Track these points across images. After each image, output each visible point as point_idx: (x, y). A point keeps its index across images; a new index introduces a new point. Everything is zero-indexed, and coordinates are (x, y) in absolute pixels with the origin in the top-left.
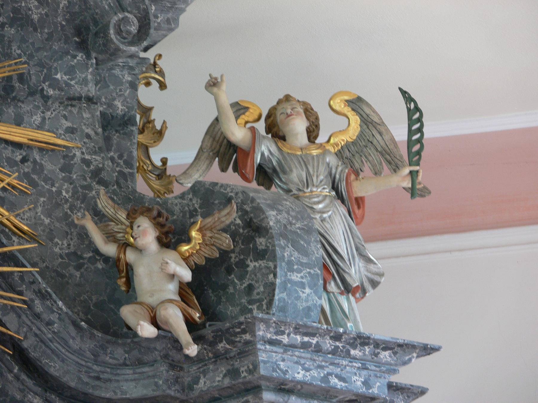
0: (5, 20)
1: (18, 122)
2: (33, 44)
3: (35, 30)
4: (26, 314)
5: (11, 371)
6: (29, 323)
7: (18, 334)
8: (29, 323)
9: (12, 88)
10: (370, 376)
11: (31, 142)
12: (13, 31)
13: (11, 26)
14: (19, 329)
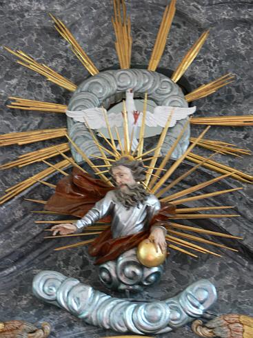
0: (222, 58)
1: (240, 113)
2: (243, 68)
3: (244, 59)
4: (243, 222)
5: (244, 266)
6: (247, 228)
7: (239, 236)
8: (247, 228)
9: (232, 97)
10: (8, 27)
11: (246, 123)
12: (228, 63)
13: (226, 61)
14: (240, 234)
